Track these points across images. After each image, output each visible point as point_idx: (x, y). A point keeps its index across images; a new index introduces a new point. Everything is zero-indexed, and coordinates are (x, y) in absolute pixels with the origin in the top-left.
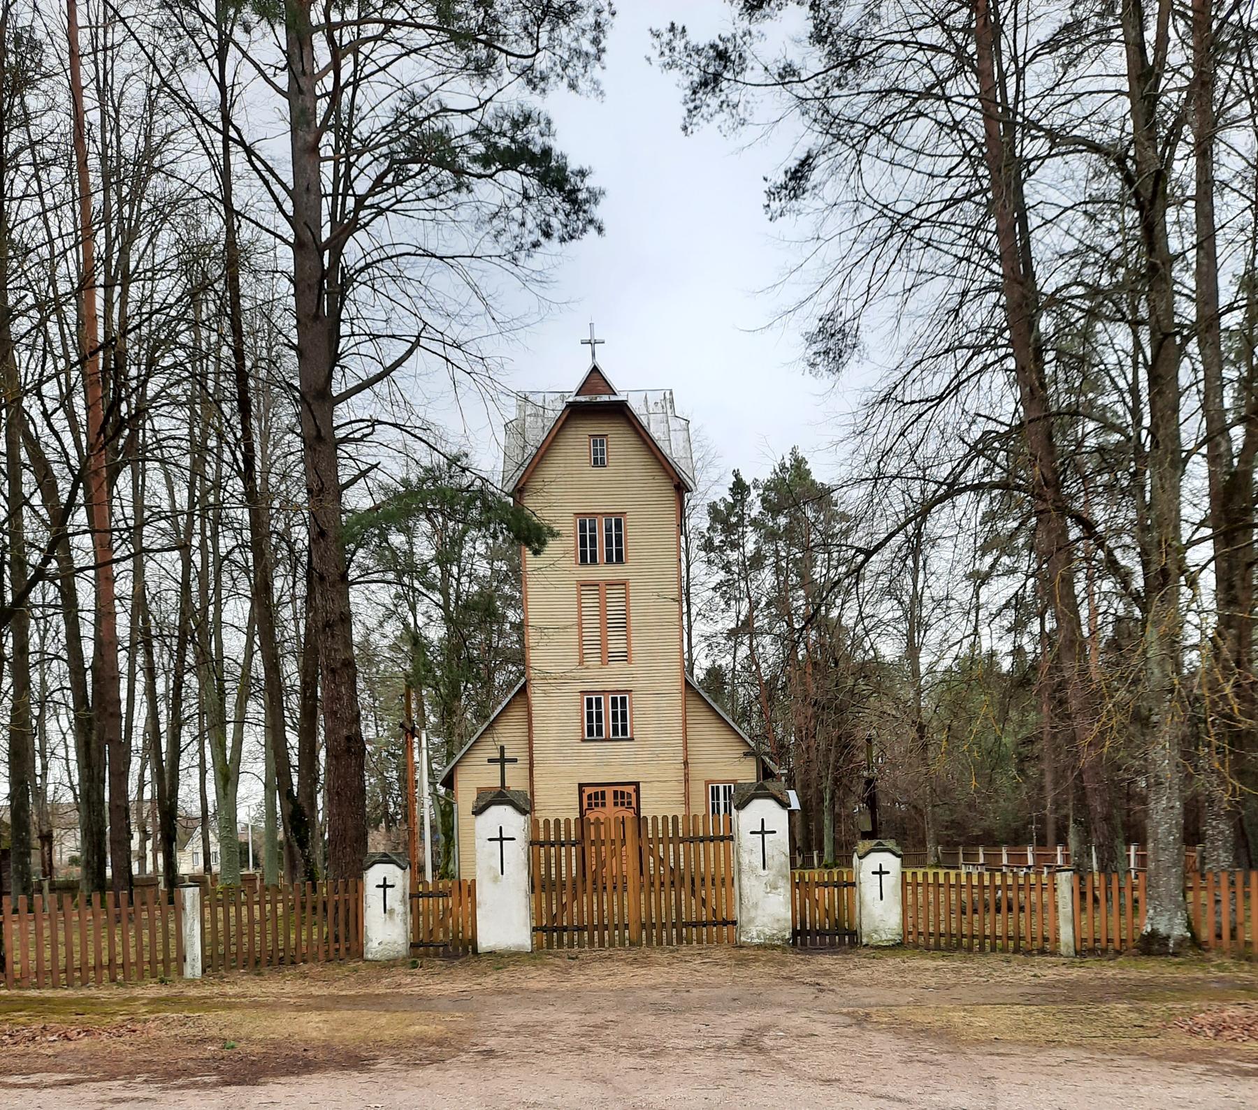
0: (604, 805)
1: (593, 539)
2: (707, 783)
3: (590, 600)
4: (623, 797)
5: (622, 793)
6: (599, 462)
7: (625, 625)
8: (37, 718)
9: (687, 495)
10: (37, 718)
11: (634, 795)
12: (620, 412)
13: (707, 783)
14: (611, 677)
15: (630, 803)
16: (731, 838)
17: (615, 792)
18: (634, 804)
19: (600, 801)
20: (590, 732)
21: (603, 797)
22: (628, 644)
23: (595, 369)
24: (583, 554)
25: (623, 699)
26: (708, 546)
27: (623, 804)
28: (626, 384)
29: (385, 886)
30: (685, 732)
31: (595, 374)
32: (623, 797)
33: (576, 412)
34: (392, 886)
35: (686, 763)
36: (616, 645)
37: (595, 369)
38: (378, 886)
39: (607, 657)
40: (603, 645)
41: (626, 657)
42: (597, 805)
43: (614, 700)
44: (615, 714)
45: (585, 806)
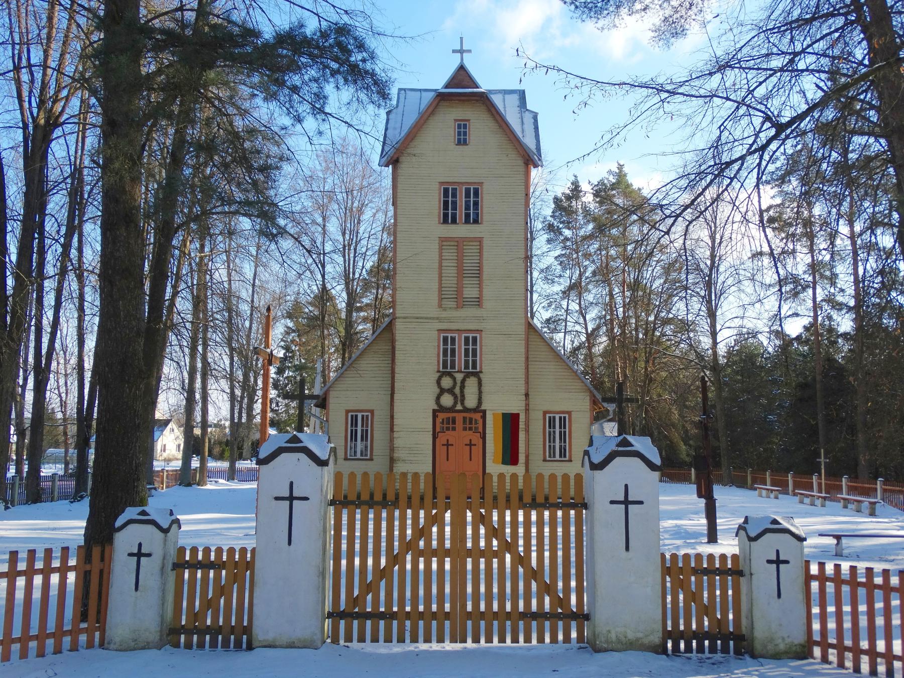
0: (454, 429)
1: (454, 203)
2: (545, 413)
3: (450, 254)
4: (471, 423)
5: (471, 419)
6: (462, 141)
7: (479, 274)
8: (21, 387)
9: (534, 172)
10: (21, 387)
11: (480, 421)
12: (483, 100)
13: (545, 413)
14: (464, 319)
15: (476, 428)
16: (585, 506)
17: (464, 418)
18: (481, 430)
19: (473, 426)
20: (563, 421)
21: (454, 422)
22: (481, 291)
23: (462, 68)
24: (446, 216)
25: (475, 339)
26: (550, 228)
27: (470, 429)
28: (486, 80)
29: (139, 555)
30: (527, 368)
31: (462, 72)
32: (471, 423)
33: (442, 98)
34: (149, 555)
35: (527, 395)
36: (470, 292)
37: (462, 68)
38: (131, 555)
39: (461, 302)
40: (459, 291)
41: (478, 302)
42: (448, 429)
43: (467, 339)
44: (467, 351)
45: (438, 429)
